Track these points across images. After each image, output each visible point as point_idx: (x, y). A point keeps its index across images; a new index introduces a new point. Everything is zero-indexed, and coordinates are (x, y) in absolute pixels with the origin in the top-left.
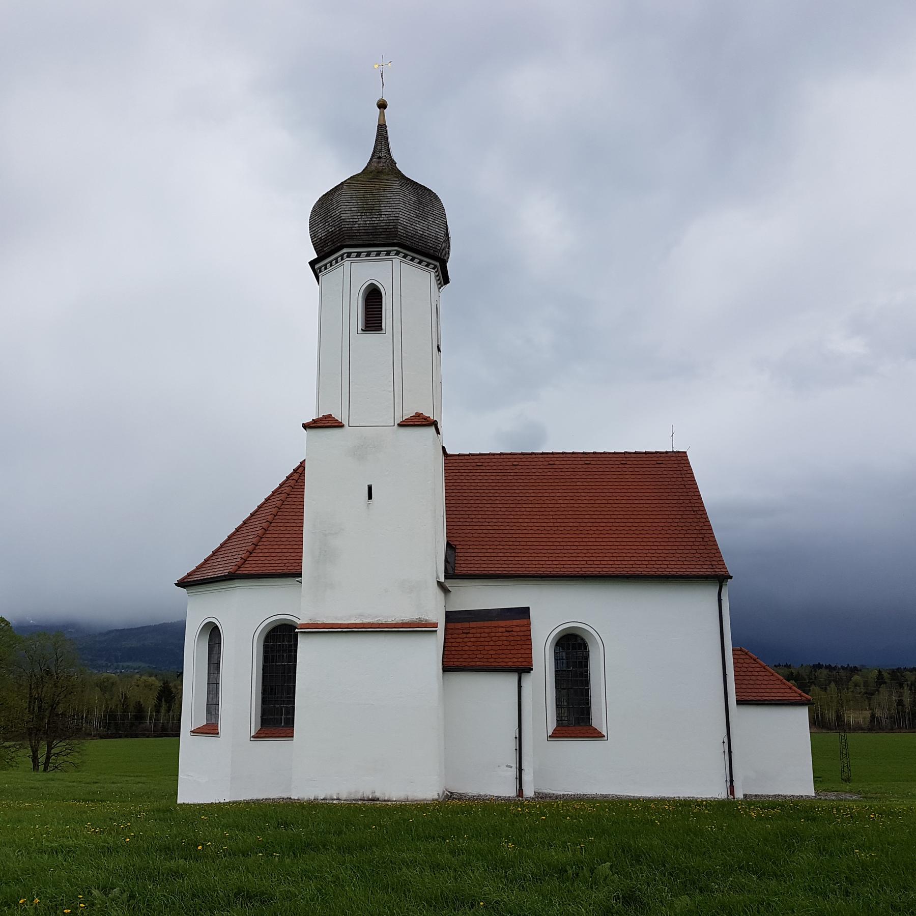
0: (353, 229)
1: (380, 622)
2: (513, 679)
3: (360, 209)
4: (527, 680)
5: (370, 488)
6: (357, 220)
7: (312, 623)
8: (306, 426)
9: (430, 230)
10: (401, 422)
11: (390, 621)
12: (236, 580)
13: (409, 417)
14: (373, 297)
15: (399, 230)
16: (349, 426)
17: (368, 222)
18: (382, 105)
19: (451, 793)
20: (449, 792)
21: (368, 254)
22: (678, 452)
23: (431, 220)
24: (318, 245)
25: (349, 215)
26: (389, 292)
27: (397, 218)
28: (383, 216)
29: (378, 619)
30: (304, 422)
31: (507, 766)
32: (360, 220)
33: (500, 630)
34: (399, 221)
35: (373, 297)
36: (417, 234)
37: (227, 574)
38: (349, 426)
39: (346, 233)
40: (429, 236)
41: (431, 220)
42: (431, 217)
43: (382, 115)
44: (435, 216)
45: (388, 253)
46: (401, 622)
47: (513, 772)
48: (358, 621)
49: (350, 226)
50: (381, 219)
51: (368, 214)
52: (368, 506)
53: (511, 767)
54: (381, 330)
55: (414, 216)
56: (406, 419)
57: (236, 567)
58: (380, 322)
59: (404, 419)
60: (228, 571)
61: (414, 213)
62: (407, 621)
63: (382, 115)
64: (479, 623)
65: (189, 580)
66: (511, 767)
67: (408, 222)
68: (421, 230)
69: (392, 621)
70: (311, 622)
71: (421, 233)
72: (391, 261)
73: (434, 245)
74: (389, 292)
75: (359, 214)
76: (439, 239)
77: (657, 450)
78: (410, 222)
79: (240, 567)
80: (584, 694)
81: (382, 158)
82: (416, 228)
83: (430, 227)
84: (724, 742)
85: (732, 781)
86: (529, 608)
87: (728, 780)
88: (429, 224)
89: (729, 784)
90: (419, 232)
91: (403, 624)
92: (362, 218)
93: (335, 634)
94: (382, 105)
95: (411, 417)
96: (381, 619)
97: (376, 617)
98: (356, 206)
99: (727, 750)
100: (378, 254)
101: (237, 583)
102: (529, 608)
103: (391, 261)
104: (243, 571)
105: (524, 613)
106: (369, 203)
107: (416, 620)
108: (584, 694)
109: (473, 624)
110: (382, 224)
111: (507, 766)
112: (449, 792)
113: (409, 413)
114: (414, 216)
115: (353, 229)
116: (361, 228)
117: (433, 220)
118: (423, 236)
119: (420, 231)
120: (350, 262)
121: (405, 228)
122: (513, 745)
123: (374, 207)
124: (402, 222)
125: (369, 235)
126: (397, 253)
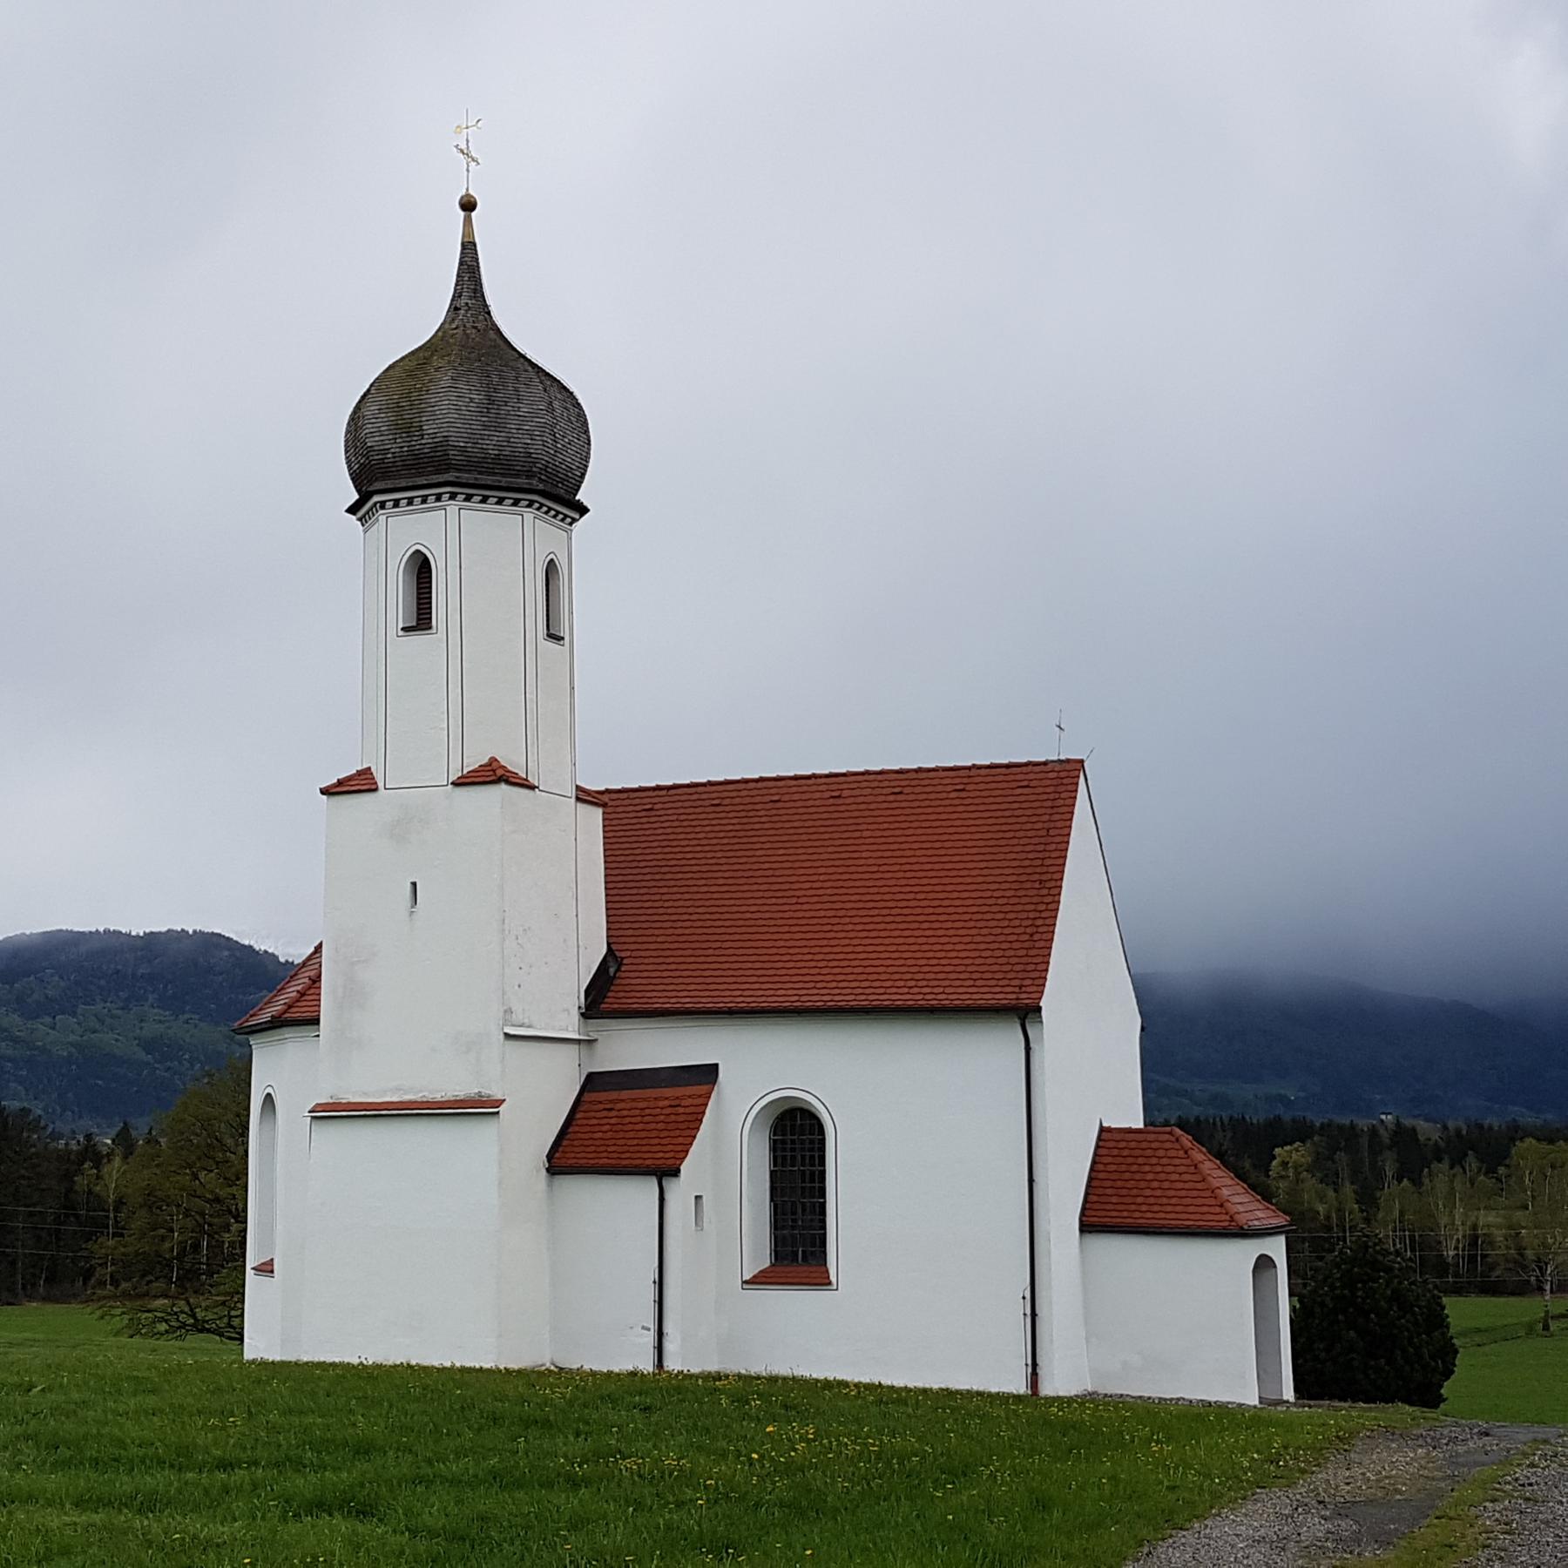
0: (386, 461)
1: (425, 1100)
2: (651, 1185)
3: (392, 427)
4: (672, 1186)
5: (414, 884)
6: (389, 446)
7: (334, 1103)
8: (324, 791)
9: (515, 445)
10: (459, 778)
11: (438, 1097)
12: (285, 1029)
13: (477, 766)
14: (421, 569)
15: (451, 457)
16: (385, 789)
17: (406, 449)
18: (468, 205)
19: (561, 1369)
20: (557, 1367)
21: (410, 502)
22: (1068, 761)
23: (513, 426)
24: (357, 479)
25: (377, 439)
26: (441, 565)
27: (446, 439)
28: (426, 437)
29: (421, 1095)
30: (322, 786)
31: (643, 1328)
32: (394, 446)
33: (661, 1104)
34: (451, 443)
35: (421, 569)
36: (487, 456)
37: (269, 1019)
38: (385, 789)
39: (377, 469)
40: (513, 454)
41: (513, 426)
42: (514, 422)
43: (468, 222)
44: (521, 418)
45: (438, 498)
46: (454, 1098)
47: (650, 1338)
48: (395, 1099)
49: (380, 457)
50: (423, 442)
51: (404, 435)
52: (410, 915)
53: (649, 1330)
54: (430, 628)
55: (479, 427)
56: (469, 772)
57: (285, 1007)
58: (428, 616)
59: (465, 772)
60: (270, 1015)
61: (478, 423)
62: (462, 1098)
63: (468, 222)
64: (695, 1088)
65: (250, 1023)
66: (649, 1330)
67: (467, 440)
68: (496, 448)
69: (442, 1097)
70: (331, 1101)
71: (496, 452)
72: (444, 511)
73: (524, 466)
74: (441, 565)
75: (391, 437)
76: (533, 456)
77: (1031, 760)
78: (472, 441)
79: (290, 1007)
80: (817, 1210)
81: (460, 309)
82: (485, 446)
83: (512, 440)
84: (1024, 1298)
85: (1035, 1365)
86: (717, 1065)
87: (1029, 1362)
88: (510, 435)
89: (1030, 1370)
90: (491, 452)
91: (456, 1101)
92: (395, 443)
93: (330, 1121)
94: (468, 205)
95: (481, 766)
96: (426, 1094)
97: (421, 1091)
98: (387, 424)
99: (1028, 1312)
100: (424, 500)
101: (288, 1033)
102: (717, 1065)
103: (444, 511)
104: (294, 1014)
105: (708, 1074)
106: (404, 417)
107: (472, 1095)
108: (817, 1210)
109: (625, 1094)
110: (426, 451)
111: (643, 1328)
112: (557, 1367)
113: (473, 763)
114: (479, 427)
115: (386, 461)
116: (397, 459)
117: (517, 427)
118: (502, 457)
119: (493, 450)
120: (384, 517)
121: (463, 450)
122: (650, 1293)
123: (411, 423)
124: (456, 444)
125: (410, 469)
126: (453, 496)
